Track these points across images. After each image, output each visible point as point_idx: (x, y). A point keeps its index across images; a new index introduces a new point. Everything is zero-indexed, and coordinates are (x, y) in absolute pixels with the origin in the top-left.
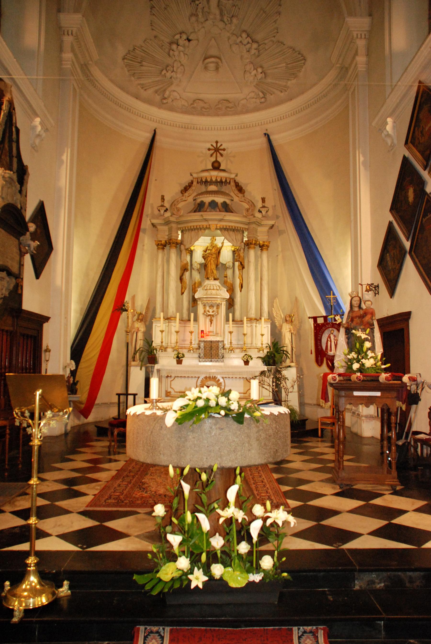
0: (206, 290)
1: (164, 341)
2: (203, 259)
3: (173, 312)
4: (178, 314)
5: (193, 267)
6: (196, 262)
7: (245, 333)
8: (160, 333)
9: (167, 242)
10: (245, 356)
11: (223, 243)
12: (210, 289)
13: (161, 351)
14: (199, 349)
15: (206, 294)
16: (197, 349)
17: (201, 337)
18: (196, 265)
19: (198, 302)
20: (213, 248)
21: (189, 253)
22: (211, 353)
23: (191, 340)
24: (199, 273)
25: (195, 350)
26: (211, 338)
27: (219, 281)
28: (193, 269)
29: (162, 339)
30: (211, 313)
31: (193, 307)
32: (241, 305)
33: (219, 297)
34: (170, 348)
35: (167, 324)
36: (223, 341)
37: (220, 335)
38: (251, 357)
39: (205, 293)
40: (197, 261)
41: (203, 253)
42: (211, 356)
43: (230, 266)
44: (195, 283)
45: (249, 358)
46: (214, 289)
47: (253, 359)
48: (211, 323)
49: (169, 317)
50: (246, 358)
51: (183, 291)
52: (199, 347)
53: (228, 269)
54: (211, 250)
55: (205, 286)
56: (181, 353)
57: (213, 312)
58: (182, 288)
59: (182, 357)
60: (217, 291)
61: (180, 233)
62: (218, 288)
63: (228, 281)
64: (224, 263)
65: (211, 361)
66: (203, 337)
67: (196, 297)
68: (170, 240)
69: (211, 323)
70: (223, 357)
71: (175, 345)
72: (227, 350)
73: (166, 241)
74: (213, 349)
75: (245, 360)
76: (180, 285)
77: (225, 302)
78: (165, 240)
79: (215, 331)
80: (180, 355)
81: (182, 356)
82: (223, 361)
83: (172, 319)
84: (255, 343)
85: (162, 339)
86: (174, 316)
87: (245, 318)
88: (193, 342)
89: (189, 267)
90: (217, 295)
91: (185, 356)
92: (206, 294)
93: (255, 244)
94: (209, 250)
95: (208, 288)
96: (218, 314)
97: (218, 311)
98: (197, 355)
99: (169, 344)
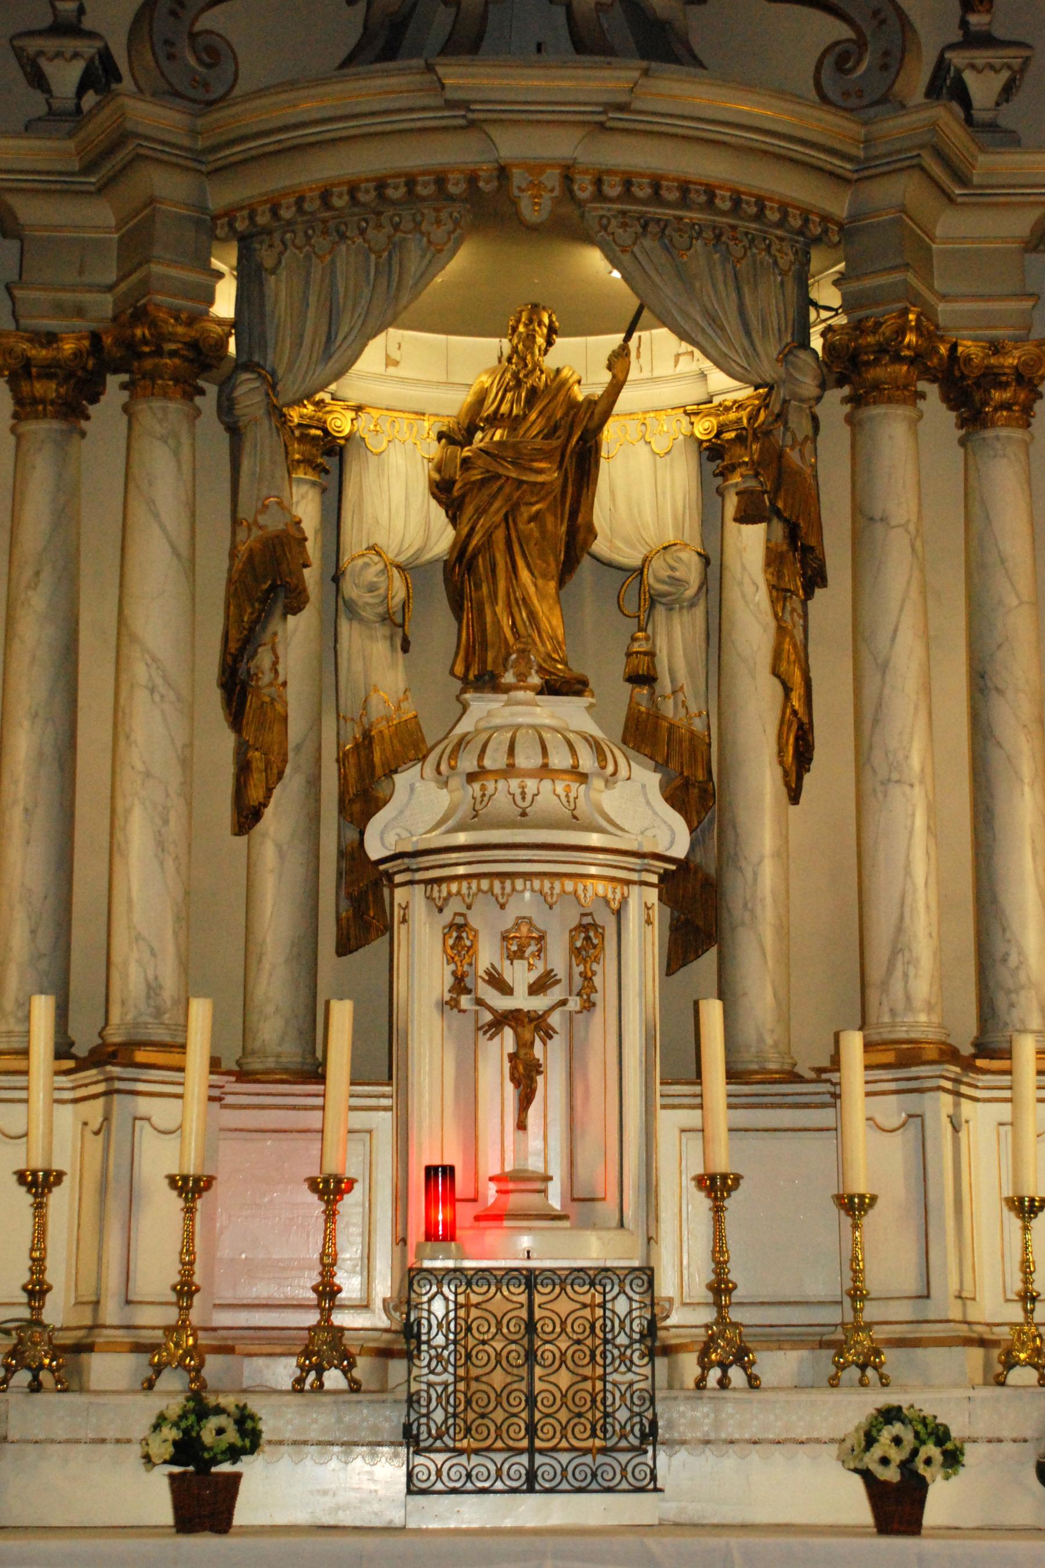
0: (471, 777)
1: (56, 1274)
2: (438, 514)
3: (153, 989)
4: (200, 1012)
5: (350, 589)
6: (373, 548)
7: (860, 1186)
8: (24, 1199)
9: (108, 341)
10: (886, 1434)
11: (619, 360)
12: (510, 771)
13: (23, 1377)
14: (410, 1356)
15: (475, 819)
16: (385, 1353)
17: (431, 1235)
18: (371, 575)
19: (400, 894)
20: (530, 403)
21: (308, 462)
22: (531, 1401)
23: (328, 1265)
24: (405, 649)
25: (363, 1368)
26: (525, 1241)
27: (585, 701)
28: (352, 610)
29: (38, 1265)
30: (521, 1001)
31: (344, 948)
32: (783, 931)
33: (595, 839)
34: (112, 1347)
35: (94, 1110)
36: (647, 1275)
37: (608, 1209)
38: (941, 1435)
39: (465, 809)
40: (380, 539)
41: (435, 449)
42: (532, 1430)
43: (674, 581)
44: (367, 738)
45: (931, 1450)
46: (545, 771)
47: (972, 1454)
48: (525, 1101)
49: (115, 1036)
50: (897, 1456)
51: (255, 794)
52: (410, 1331)
53: (660, 612)
54: (513, 422)
55: (462, 742)
56: (228, 1401)
57: (536, 989)
58: (243, 769)
59: (234, 1454)
60: (578, 790)
61: (225, 261)
62: (587, 762)
63: (669, 709)
64: (631, 558)
65: (531, 1484)
66: (450, 1235)
67: (375, 850)
68: (140, 315)
69: (525, 1101)
70: (650, 1435)
71: (171, 1316)
72: (689, 1365)
73: (95, 337)
74: (547, 1351)
75: (891, 1474)
76: (228, 740)
77: (652, 895)
78: (83, 325)
79: (557, 1170)
80: (208, 1437)
81: (232, 1436)
82: (650, 1485)
83: (141, 1056)
84: (953, 1286)
85: (38, 1265)
86: (161, 1034)
87: (854, 1043)
88: (350, 1286)
89: (311, 576)
90: (575, 822)
91: (268, 1428)
92: (475, 819)
93: (917, 359)
94: (495, 420)
95: (494, 760)
96: (589, 1006)
97: (587, 978)
98: (392, 1418)
99: (111, 1313)
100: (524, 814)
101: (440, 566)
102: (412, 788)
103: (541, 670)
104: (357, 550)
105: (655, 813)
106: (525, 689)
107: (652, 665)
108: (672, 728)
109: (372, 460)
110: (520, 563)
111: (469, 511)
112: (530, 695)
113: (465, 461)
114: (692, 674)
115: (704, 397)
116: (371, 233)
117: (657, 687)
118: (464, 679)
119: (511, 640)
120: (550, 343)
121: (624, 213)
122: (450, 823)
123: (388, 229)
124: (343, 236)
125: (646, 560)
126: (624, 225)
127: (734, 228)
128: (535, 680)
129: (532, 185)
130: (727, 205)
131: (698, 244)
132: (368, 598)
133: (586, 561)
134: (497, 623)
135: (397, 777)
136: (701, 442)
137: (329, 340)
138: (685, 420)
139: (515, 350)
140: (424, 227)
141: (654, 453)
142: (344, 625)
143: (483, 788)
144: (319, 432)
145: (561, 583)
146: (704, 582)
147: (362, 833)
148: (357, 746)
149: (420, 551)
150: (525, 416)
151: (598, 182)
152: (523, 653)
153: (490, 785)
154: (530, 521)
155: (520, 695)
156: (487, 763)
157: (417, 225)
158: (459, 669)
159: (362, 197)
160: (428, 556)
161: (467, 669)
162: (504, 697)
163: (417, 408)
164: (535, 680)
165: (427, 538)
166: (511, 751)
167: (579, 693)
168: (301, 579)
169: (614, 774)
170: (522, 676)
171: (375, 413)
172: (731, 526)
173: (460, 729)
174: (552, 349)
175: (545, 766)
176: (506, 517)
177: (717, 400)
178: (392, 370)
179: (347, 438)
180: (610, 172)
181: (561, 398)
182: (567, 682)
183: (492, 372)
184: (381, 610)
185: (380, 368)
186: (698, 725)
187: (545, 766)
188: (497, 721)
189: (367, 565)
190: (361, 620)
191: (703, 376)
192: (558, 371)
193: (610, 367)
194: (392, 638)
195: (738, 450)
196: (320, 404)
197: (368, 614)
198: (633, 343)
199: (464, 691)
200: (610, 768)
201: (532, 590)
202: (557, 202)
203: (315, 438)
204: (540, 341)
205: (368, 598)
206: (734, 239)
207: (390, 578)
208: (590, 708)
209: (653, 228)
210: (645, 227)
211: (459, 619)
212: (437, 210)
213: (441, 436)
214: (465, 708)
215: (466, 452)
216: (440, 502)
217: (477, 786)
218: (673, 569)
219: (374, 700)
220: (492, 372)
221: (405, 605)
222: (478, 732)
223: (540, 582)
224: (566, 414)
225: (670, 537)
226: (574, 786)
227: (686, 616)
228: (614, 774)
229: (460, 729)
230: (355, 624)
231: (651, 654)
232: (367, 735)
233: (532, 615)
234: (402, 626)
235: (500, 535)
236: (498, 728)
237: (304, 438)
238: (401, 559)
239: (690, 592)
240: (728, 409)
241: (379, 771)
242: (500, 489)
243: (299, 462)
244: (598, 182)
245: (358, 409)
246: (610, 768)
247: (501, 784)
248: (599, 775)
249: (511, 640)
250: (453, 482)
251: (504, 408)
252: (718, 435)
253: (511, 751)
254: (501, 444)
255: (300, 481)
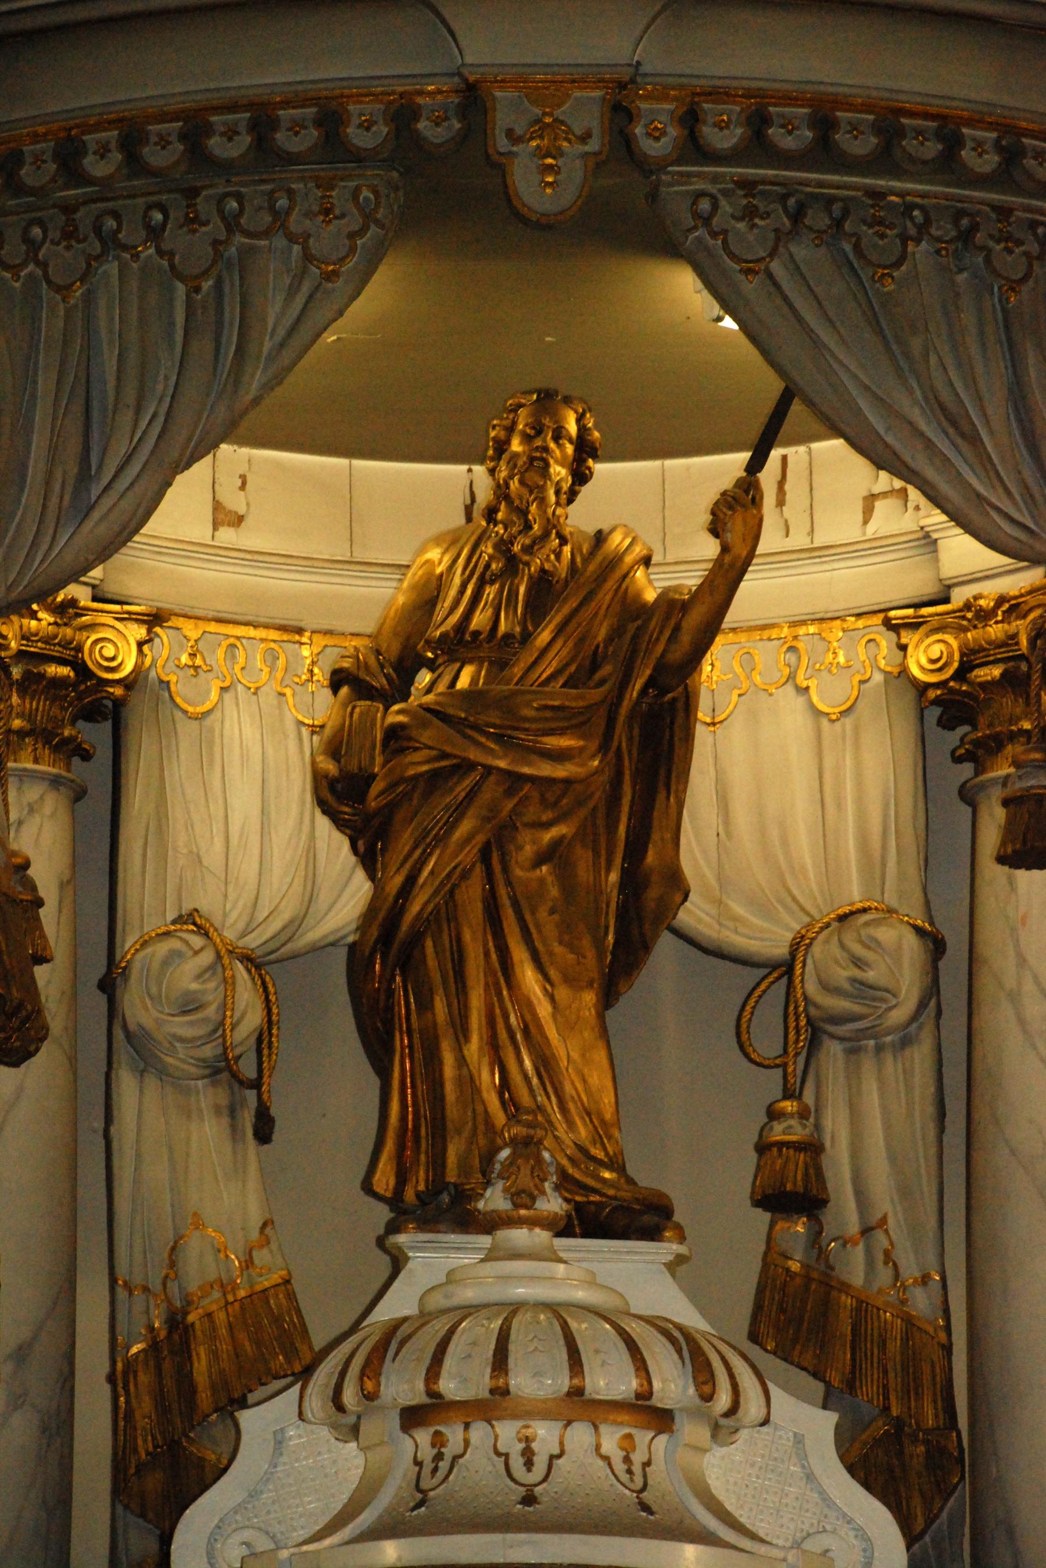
27: (667, 1249)
43: (862, 989)
53: (833, 1051)
100: (529, 1499)
101: (340, 958)
102: (279, 1442)
103: (566, 1183)
104: (152, 925)
105: (826, 1500)
106: (532, 1223)
107: (816, 1173)
108: (863, 1309)
109: (187, 730)
110: (519, 954)
111: (404, 840)
112: (541, 1236)
113: (394, 733)
114: (905, 1192)
115: (929, 589)
116: (176, 238)
117: (828, 1216)
118: (395, 1201)
119: (500, 1118)
120: (581, 476)
121: (748, 186)
122: (366, 1519)
123: (215, 227)
124: (110, 243)
125: (800, 944)
126: (749, 214)
127: (1004, 212)
128: (552, 1204)
129: (539, 127)
130: (988, 162)
131: (921, 251)
132: (182, 1027)
133: (665, 945)
134: (469, 1084)
135: (246, 1418)
136: (922, 688)
137: (85, 475)
138: (885, 641)
139: (502, 492)
140: (296, 223)
141: (817, 713)
142: (126, 1083)
143: (439, 1440)
144: (64, 671)
145: (608, 998)
146: (932, 990)
147: (166, 1540)
148: (154, 1347)
149: (295, 926)
150: (526, 637)
151: (691, 119)
152: (528, 1147)
153: (454, 1434)
154: (540, 859)
155: (519, 1236)
156: (449, 1386)
157: (280, 217)
158: (384, 1180)
159: (154, 156)
160: (314, 934)
161: (402, 1178)
162: (485, 1241)
163: (290, 617)
164: (552, 1204)
165: (310, 899)
166: (500, 1361)
167: (652, 1234)
168: (31, 987)
169: (733, 1410)
170: (522, 1197)
171: (191, 630)
172: (992, 872)
173: (385, 1312)
174: (585, 491)
175: (577, 1393)
176: (485, 855)
177: (960, 596)
178: (227, 535)
179: (129, 684)
180: (719, 94)
181: (605, 596)
182: (623, 1208)
183: (451, 540)
184: (209, 1051)
185: (200, 530)
186: (922, 1303)
187: (577, 1393)
188: (469, 1294)
189: (174, 955)
190: (163, 1073)
191: (928, 542)
192: (600, 538)
193: (715, 530)
194: (232, 1112)
195: (1008, 703)
196: (67, 610)
197: (178, 1060)
198: (768, 477)
199: (393, 1228)
200: (723, 1400)
201: (544, 1010)
202: (598, 165)
203: (57, 682)
204: (559, 472)
205: (182, 1027)
206: (1005, 238)
207: (229, 983)
208: (674, 1266)
209: (817, 219)
210: (797, 217)
211: (381, 1064)
212: (327, 185)
213: (338, 680)
214: (397, 1263)
215: (396, 715)
216: (338, 822)
217: (423, 1436)
218: (858, 962)
219: (194, 1247)
220: (451, 540)
221: (263, 1040)
222: (425, 1317)
223: (563, 993)
224: (616, 633)
225: (855, 894)
226: (643, 1437)
227: (890, 1065)
228: (733, 1410)
229: (385, 1312)
230: (151, 1081)
231: (813, 1148)
232: (176, 1322)
233: (545, 1063)
234: (256, 1085)
235: (472, 894)
236: (468, 1311)
237: (31, 683)
238: (253, 941)
239: (899, 1015)
240: (984, 616)
241: (204, 1398)
242: (471, 795)
243: (22, 734)
244: (691, 119)
245: (154, 619)
246: (723, 1400)
247: (479, 1432)
248: (694, 1414)
249: (500, 1118)
250: (370, 778)
251: (480, 620)
252: (961, 674)
253: (500, 1361)
254: (471, 696)
255: (24, 775)
